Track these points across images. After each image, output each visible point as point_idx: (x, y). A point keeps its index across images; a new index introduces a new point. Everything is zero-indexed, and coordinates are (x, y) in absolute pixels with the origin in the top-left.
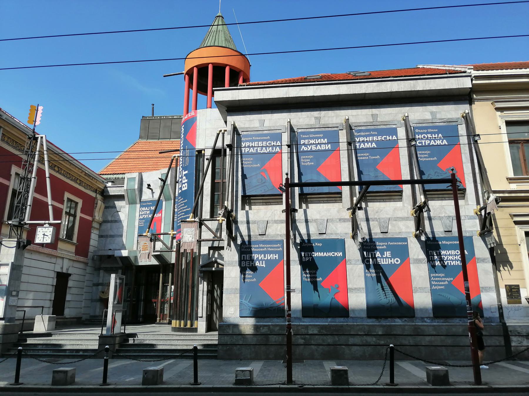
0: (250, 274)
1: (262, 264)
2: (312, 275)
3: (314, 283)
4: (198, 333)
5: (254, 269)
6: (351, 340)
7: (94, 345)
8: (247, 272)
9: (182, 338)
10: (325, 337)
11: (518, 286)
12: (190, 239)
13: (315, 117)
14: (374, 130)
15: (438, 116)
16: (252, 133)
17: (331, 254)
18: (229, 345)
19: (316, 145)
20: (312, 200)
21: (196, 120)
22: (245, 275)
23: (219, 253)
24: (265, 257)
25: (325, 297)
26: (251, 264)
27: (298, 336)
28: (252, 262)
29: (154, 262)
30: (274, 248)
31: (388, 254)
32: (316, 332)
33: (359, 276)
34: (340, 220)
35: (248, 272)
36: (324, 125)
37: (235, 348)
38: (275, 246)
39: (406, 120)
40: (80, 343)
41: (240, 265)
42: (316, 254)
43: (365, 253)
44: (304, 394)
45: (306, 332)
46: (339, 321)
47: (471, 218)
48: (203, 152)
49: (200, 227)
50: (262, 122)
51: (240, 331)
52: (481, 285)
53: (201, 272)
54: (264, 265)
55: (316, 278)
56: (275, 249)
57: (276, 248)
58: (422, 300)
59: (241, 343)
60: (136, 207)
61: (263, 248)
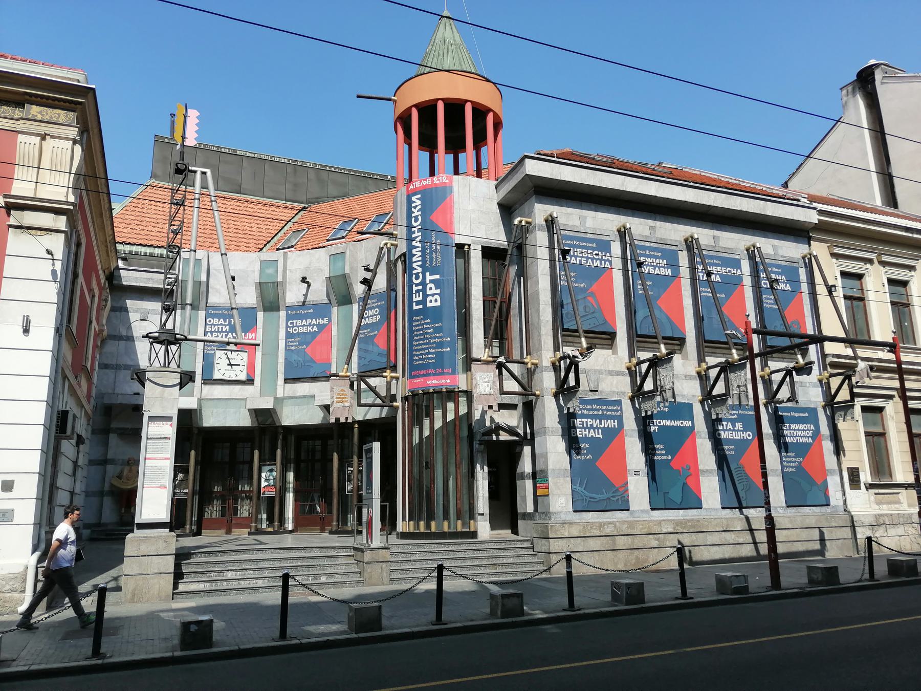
4: (479, 539)
9: (463, 547)
11: (858, 469)
15: (781, 252)
16: (572, 234)
17: (678, 423)
21: (451, 191)
24: (601, 423)
27: (651, 536)
29: (245, 421)
31: (739, 426)
34: (686, 376)
36: (661, 239)
38: (612, 408)
39: (550, 223)
40: (299, 564)
44: (430, 639)
47: (688, 377)
49: (501, 373)
50: (583, 219)
52: (701, 467)
54: (601, 436)
56: (613, 413)
57: (614, 411)
61: (598, 410)
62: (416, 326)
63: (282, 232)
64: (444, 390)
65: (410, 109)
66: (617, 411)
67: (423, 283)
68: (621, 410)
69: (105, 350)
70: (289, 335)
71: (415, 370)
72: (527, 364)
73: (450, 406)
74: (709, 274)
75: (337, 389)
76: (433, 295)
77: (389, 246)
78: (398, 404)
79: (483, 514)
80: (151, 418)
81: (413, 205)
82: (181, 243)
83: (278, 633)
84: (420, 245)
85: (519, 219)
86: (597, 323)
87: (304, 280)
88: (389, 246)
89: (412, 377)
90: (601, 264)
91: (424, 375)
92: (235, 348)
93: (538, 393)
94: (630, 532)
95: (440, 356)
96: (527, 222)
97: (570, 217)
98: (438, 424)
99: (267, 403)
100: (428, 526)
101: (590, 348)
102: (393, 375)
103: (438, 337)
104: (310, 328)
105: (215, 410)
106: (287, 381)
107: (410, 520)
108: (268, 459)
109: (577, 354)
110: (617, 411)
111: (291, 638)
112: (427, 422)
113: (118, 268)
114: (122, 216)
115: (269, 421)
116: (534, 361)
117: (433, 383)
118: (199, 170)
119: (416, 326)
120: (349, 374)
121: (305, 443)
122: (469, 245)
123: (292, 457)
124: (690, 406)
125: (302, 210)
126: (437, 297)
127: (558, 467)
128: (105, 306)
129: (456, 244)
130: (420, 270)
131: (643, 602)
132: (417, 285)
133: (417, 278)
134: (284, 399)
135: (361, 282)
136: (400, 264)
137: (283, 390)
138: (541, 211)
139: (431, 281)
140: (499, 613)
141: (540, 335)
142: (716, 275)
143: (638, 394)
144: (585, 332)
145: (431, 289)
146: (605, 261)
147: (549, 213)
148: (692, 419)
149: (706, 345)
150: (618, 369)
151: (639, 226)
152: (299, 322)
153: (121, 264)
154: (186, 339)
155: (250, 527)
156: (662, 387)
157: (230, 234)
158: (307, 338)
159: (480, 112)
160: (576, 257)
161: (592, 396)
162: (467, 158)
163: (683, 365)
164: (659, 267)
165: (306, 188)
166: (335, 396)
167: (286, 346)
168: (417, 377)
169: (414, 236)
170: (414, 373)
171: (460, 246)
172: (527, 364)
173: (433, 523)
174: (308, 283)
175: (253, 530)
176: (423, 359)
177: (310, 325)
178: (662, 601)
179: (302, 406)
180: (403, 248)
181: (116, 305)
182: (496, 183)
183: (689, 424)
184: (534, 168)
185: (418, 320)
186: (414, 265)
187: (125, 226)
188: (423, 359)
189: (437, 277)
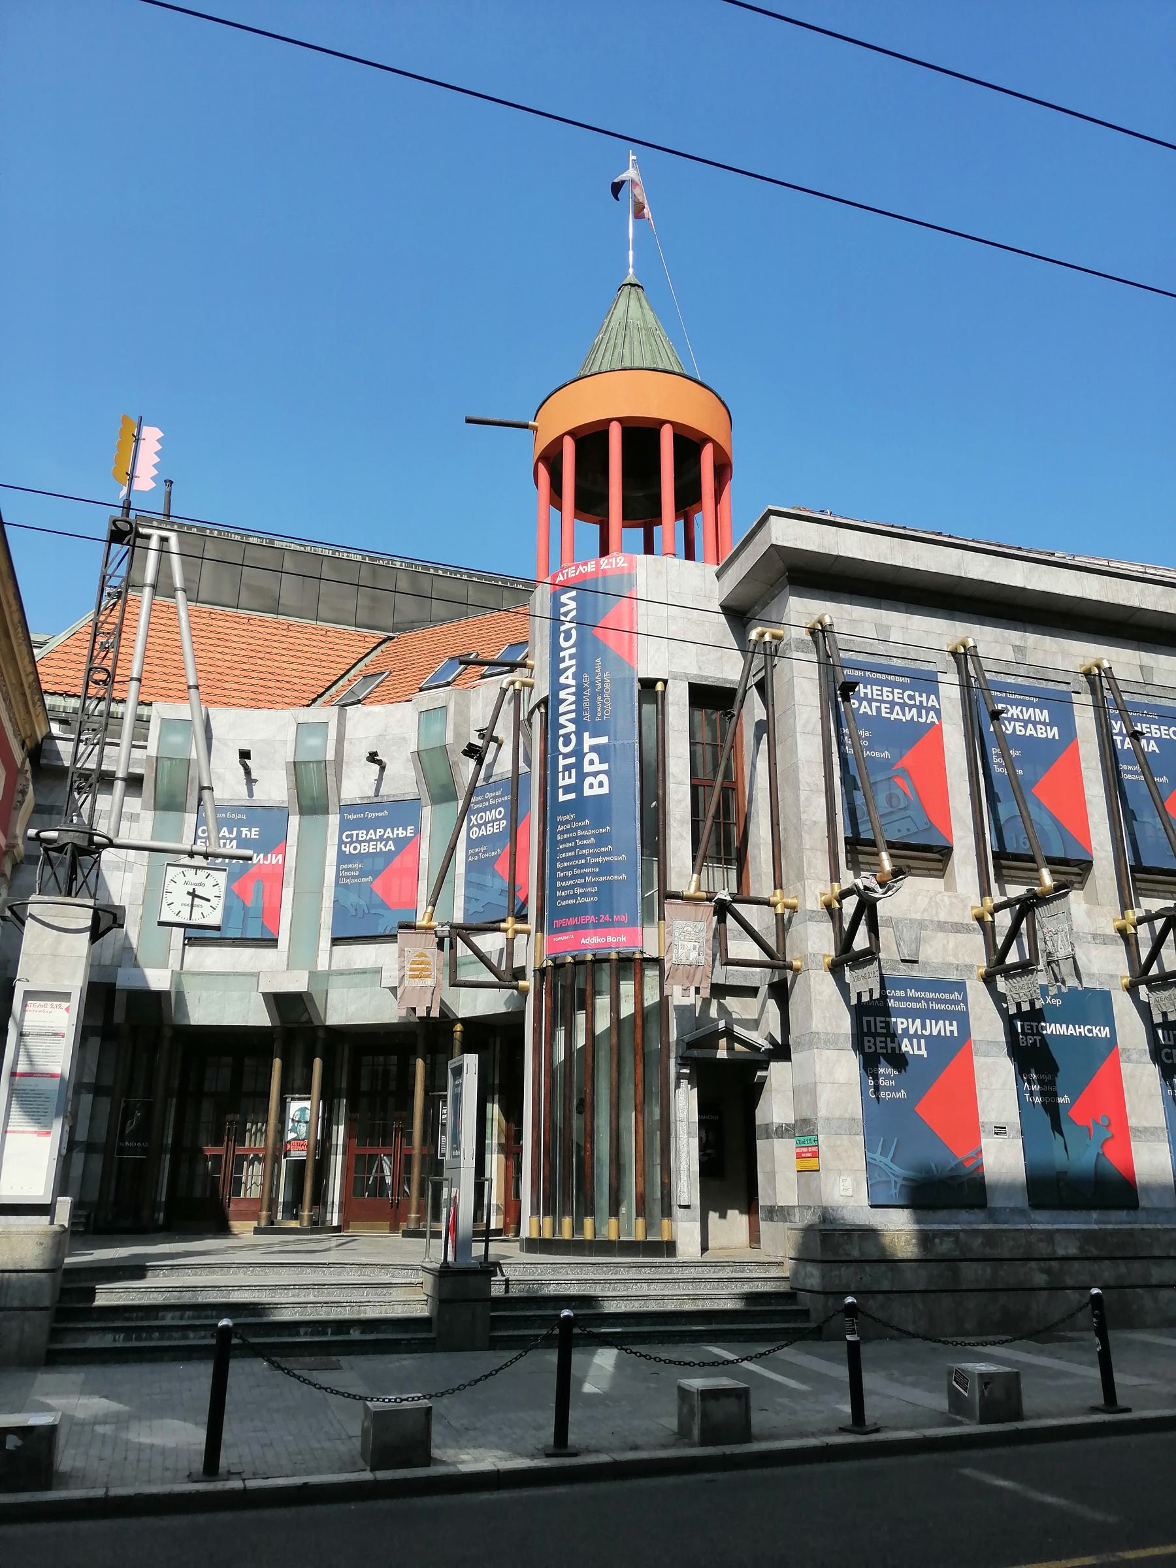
0: (888, 1077)
1: (919, 1049)
2: (1046, 1088)
3: (1052, 1109)
5: (899, 1061)
6: (1158, 1273)
7: (412, 1301)
8: (881, 1071)
9: (646, 1274)
10: (1096, 1266)
12: (693, 955)
13: (1014, 647)
14: (1149, 707)
17: (1083, 1030)
18: (837, 1297)
19: (1026, 723)
20: (1012, 872)
22: (876, 1077)
23: (720, 1004)
24: (924, 1027)
25: (1079, 1154)
26: (890, 1045)
27: (1033, 1264)
28: (893, 1042)
29: (260, 1017)
30: (945, 1002)
32: (1073, 1251)
33: (1151, 1096)
34: (1095, 936)
35: (884, 1070)
37: (871, 1302)
38: (947, 996)
39: (820, 633)
40: (311, 1298)
41: (858, 1043)
42: (1051, 1028)
43: (1160, 1032)
45: (1049, 1250)
46: (1116, 1221)
47: (1099, 938)
48: (659, 686)
49: (722, 920)
51: (882, 1248)
52: (1132, 1122)
53: (683, 1061)
54: (924, 1052)
55: (1055, 1095)
56: (949, 1008)
58: (1003, 1158)
59: (886, 1286)
60: (182, 821)
61: (918, 1000)
62: (563, 832)
63: (346, 678)
64: (614, 956)
65: (558, 442)
66: (956, 1002)
67: (578, 753)
68: (965, 1001)
69: (18, 882)
70: (342, 858)
71: (551, 916)
72: (774, 905)
73: (627, 988)
74: (1136, 736)
75: (411, 952)
76: (595, 774)
77: (517, 686)
78: (529, 983)
79: (687, 1207)
80: (29, 995)
81: (563, 610)
82: (115, 667)
83: (198, 1465)
84: (573, 682)
85: (759, 629)
86: (913, 830)
87: (373, 757)
88: (517, 686)
89: (555, 931)
90: (920, 716)
91: (576, 928)
92: (204, 863)
93: (796, 964)
94: (988, 1252)
95: (606, 890)
96: (774, 637)
97: (857, 623)
98: (603, 1023)
99: (297, 983)
100: (578, 1227)
101: (898, 873)
102: (519, 926)
103: (604, 854)
104: (380, 846)
105: (204, 994)
106: (335, 941)
107: (545, 1215)
108: (294, 1087)
109: (872, 883)
110: (956, 1002)
111: (230, 1475)
112: (581, 1018)
113: (50, 737)
114: (67, 649)
115: (304, 1018)
116: (790, 901)
117: (592, 942)
118: (156, 534)
119: (563, 832)
120: (434, 923)
121: (367, 1059)
122: (665, 682)
123: (344, 1085)
124: (1105, 997)
125: (384, 641)
126: (603, 778)
127: (837, 1114)
128: (21, 803)
129: (640, 680)
130: (572, 728)
131: (1018, 1416)
132: (566, 756)
133: (566, 744)
134: (329, 974)
135: (465, 753)
136: (537, 716)
137: (327, 957)
138: (801, 610)
139: (593, 749)
140: (696, 1431)
141: (800, 850)
142: (1148, 739)
143: (996, 968)
144: (891, 845)
145: (593, 763)
146: (928, 710)
147: (816, 617)
148: (1109, 1021)
149: (1138, 875)
150: (957, 919)
151: (994, 643)
152: (362, 834)
153: (55, 729)
154: (111, 844)
155: (258, 1218)
156: (1049, 954)
157: (253, 681)
158: (375, 864)
159: (689, 445)
160: (870, 701)
161: (905, 971)
162: (669, 529)
163: (1089, 914)
164: (1035, 723)
165: (398, 603)
166: (408, 966)
167: (338, 877)
168: (563, 930)
169: (562, 666)
170: (557, 923)
171: (648, 685)
172: (774, 905)
173: (588, 1222)
174: (380, 762)
175: (263, 1223)
176: (574, 896)
177: (381, 839)
178: (1061, 1414)
179: (369, 989)
180: (542, 689)
181: (41, 802)
182: (716, 568)
183: (1105, 1032)
184: (786, 534)
185: (567, 822)
186: (562, 720)
187: (72, 665)
188: (574, 896)
189: (604, 740)
